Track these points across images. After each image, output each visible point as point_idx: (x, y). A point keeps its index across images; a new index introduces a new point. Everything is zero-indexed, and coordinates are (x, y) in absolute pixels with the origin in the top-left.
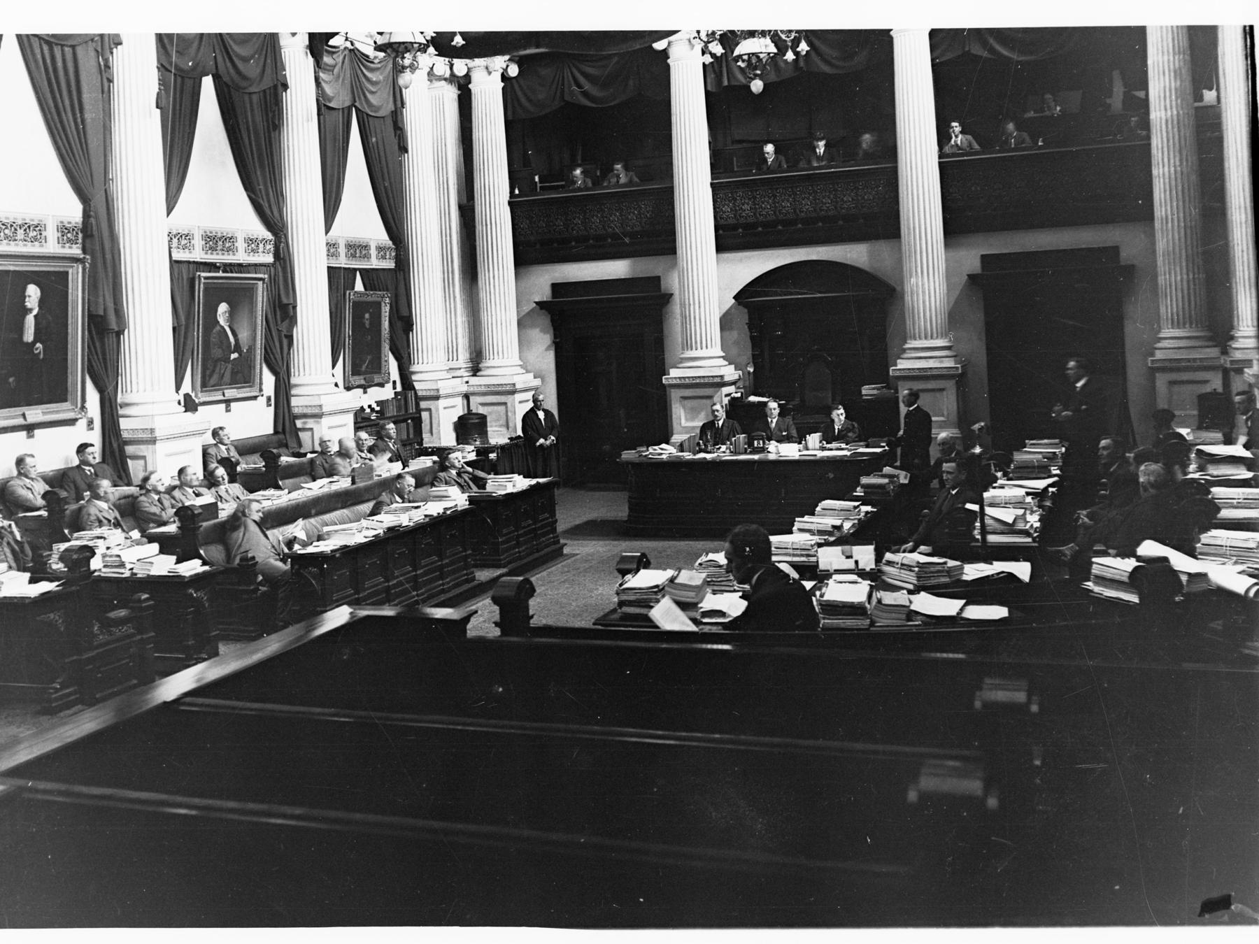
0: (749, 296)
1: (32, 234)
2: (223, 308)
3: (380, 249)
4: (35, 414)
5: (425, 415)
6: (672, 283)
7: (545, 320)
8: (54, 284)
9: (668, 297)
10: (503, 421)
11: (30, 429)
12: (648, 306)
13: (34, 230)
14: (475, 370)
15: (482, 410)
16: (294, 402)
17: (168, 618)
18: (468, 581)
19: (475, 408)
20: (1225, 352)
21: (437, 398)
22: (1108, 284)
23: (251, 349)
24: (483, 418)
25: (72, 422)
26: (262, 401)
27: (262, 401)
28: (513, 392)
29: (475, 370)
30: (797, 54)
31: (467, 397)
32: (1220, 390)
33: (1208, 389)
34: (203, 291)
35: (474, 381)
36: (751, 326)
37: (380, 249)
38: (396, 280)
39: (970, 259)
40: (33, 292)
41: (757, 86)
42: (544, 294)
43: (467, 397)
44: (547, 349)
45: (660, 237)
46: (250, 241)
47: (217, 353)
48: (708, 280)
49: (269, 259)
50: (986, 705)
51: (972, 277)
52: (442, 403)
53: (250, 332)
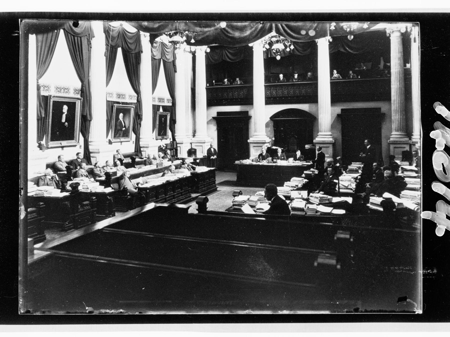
0: (275, 119)
1: (66, 91)
2: (121, 115)
3: (168, 100)
4: (64, 143)
5: (179, 148)
6: (251, 113)
7: (214, 122)
9: (250, 117)
11: (63, 147)
12: (244, 120)
13: (66, 90)
14: (194, 136)
16: (141, 143)
17: (101, 205)
18: (189, 197)
19: (194, 147)
20: (410, 139)
22: (378, 118)
23: (129, 127)
24: (195, 150)
25: (75, 146)
27: (131, 142)
28: (204, 143)
29: (194, 136)
32: (409, 150)
33: (405, 150)
34: (115, 110)
36: (274, 127)
38: (172, 109)
39: (338, 110)
40: (65, 108)
41: (278, 58)
42: (215, 115)
45: (248, 100)
46: (130, 96)
47: (119, 128)
48: (262, 114)
50: (319, 264)
51: (338, 115)
53: (129, 122)
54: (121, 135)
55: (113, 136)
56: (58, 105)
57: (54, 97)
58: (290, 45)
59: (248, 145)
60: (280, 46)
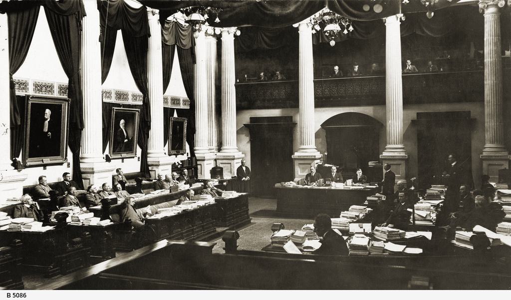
1: (108, 95)
2: (122, 121)
3: (184, 101)
4: (47, 160)
5: (199, 167)
6: (297, 119)
8: (56, 110)
10: (229, 170)
12: (287, 129)
14: (219, 150)
15: (221, 166)
21: (204, 160)
23: (133, 138)
25: (61, 164)
26: (136, 159)
27: (136, 159)
28: (234, 159)
29: (219, 150)
30: (348, 31)
31: (216, 160)
32: (507, 168)
33: (503, 168)
35: (219, 154)
37: (184, 101)
38: (190, 114)
39: (413, 114)
40: (48, 112)
41: (333, 43)
43: (216, 160)
44: (248, 142)
45: (292, 100)
48: (311, 118)
49: (141, 103)
52: (205, 162)
53: (134, 132)
54: (123, 149)
55: (27, 154)
56: (39, 109)
57: (33, 97)
58: (348, 26)
59: (292, 161)
60: (334, 27)
